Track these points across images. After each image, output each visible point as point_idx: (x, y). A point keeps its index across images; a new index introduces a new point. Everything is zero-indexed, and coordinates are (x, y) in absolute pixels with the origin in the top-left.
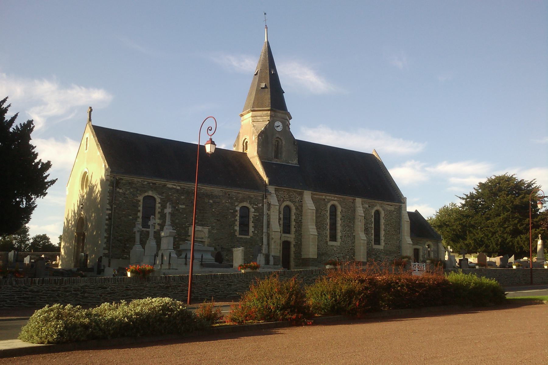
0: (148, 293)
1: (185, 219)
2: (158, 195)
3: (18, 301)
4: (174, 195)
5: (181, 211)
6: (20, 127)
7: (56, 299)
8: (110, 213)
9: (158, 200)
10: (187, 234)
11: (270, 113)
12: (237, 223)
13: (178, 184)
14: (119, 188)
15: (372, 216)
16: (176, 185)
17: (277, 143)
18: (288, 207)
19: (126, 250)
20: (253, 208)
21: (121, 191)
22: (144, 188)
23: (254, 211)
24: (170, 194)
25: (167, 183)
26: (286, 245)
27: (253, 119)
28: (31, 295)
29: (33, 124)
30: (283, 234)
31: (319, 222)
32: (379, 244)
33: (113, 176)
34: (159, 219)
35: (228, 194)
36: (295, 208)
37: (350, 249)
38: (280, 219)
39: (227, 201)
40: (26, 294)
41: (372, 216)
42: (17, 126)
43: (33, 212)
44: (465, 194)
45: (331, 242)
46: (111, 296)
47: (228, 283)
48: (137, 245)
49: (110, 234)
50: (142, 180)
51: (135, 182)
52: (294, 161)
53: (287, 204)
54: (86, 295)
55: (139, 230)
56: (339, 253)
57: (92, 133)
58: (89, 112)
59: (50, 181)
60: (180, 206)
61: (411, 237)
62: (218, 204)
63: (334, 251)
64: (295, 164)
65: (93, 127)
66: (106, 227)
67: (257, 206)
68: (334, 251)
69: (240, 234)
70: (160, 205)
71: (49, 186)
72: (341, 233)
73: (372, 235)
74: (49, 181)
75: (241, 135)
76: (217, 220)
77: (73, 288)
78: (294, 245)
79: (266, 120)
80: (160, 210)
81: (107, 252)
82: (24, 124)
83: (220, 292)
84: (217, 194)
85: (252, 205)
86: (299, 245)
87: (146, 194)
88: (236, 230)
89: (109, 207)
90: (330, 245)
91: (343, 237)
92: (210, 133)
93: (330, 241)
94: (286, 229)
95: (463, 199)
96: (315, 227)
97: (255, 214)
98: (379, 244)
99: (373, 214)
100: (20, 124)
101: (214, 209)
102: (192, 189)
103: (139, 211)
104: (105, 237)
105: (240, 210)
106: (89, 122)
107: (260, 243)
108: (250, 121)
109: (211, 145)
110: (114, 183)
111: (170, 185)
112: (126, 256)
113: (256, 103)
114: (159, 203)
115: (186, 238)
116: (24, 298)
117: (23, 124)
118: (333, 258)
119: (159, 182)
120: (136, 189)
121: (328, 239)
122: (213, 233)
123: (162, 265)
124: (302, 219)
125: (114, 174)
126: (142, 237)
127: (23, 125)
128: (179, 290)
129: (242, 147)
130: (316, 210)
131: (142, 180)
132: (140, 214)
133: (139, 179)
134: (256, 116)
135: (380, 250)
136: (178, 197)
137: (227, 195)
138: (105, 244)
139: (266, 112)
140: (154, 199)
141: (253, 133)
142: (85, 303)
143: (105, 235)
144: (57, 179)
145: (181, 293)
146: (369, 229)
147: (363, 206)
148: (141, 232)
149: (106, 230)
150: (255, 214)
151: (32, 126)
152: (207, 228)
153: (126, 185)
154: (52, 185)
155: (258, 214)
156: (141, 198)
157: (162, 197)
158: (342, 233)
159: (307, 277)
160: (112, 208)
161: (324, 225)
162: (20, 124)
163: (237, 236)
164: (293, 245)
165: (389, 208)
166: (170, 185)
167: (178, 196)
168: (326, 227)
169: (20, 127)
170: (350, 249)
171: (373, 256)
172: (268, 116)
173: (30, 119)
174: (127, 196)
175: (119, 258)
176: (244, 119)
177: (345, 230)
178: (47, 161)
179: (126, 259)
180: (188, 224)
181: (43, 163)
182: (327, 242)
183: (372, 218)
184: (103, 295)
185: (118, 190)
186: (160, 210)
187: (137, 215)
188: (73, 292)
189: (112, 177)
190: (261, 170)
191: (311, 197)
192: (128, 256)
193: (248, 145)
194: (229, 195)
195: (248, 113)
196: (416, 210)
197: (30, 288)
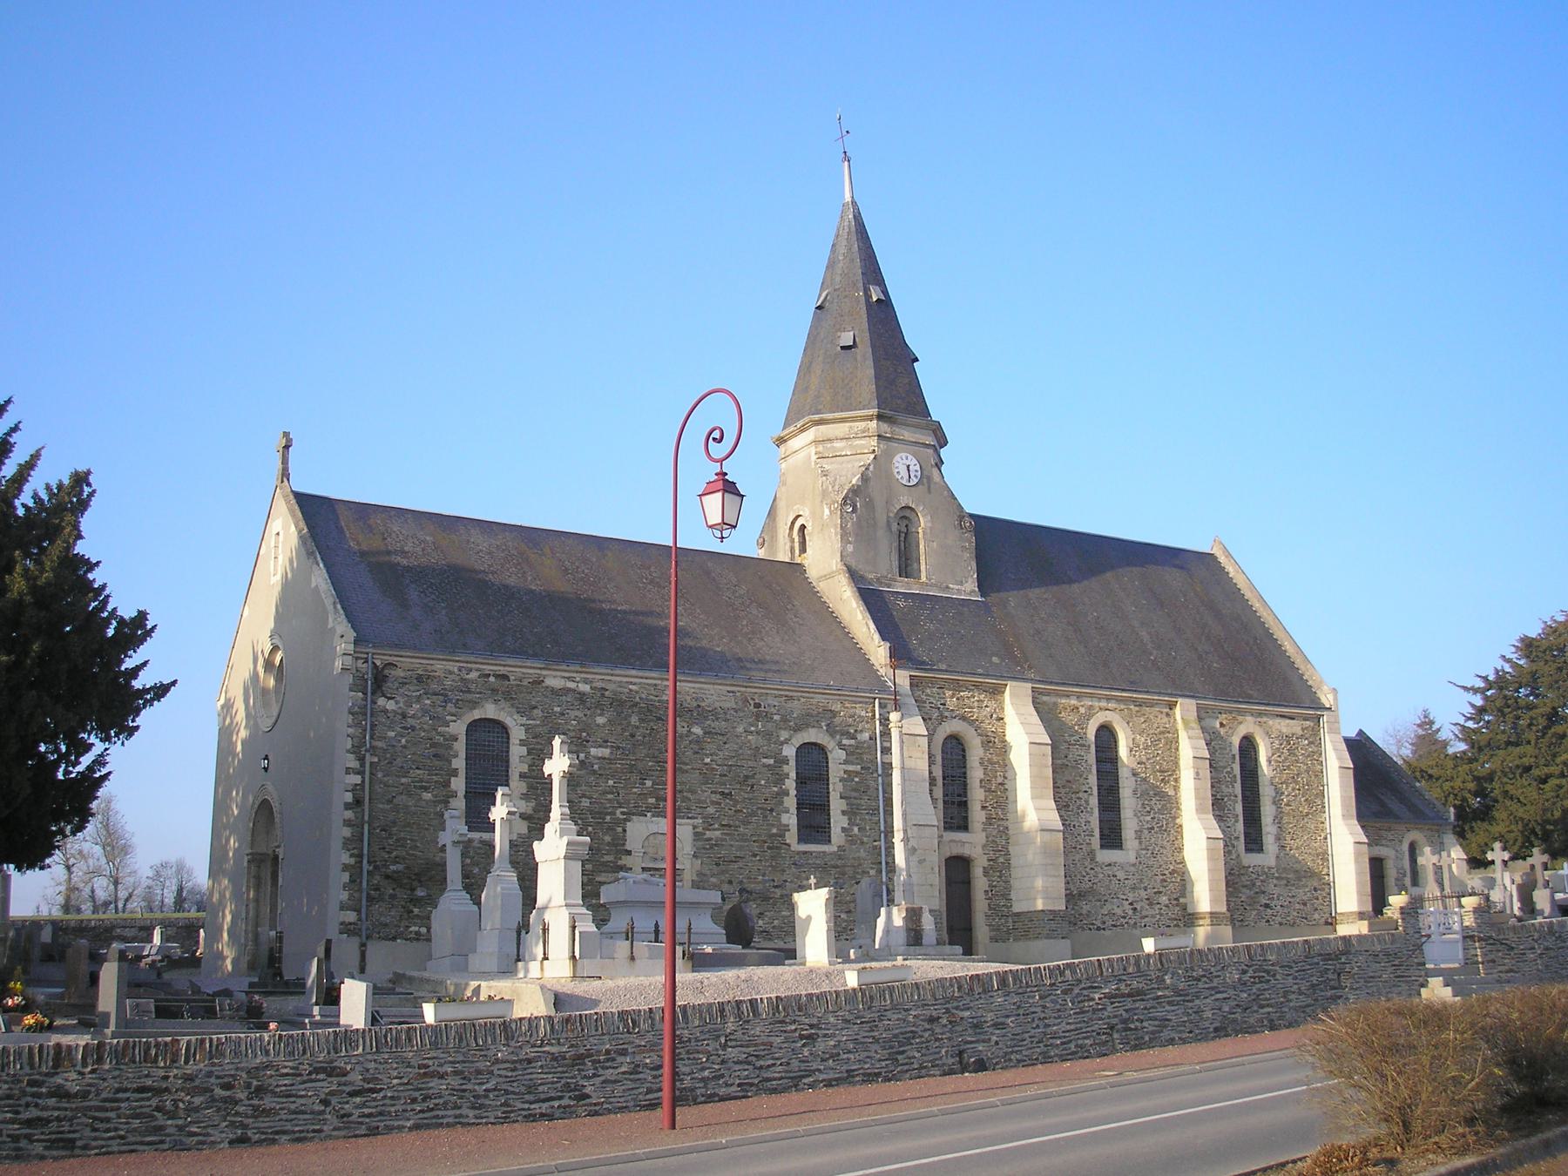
0: (504, 1087)
1: (610, 796)
2: (515, 717)
3: (8, 1136)
4: (573, 714)
5: (596, 767)
6: (45, 497)
7: (153, 1124)
8: (359, 782)
9: (517, 733)
10: (622, 850)
11: (875, 425)
12: (791, 802)
13: (583, 675)
14: (384, 696)
15: (1234, 755)
16: (578, 679)
17: (907, 526)
18: (957, 739)
19: (416, 911)
20: (841, 746)
21: (391, 705)
22: (469, 692)
23: (844, 758)
24: (557, 709)
25: (544, 672)
26: (957, 870)
27: (820, 448)
28: (58, 1109)
29: (89, 485)
30: (944, 834)
31: (1064, 787)
32: (1260, 850)
33: (366, 656)
34: (521, 798)
35: (752, 702)
36: (980, 742)
37: (1170, 873)
38: (932, 781)
39: (752, 729)
40: (36, 1105)
41: (1234, 755)
42: (36, 496)
43: (99, 794)
44: (1480, 677)
45: (1105, 852)
46: (364, 1105)
47: (803, 1030)
48: (450, 894)
49: (360, 856)
50: (462, 665)
51: (437, 674)
52: (967, 582)
53: (953, 729)
54: (268, 1102)
55: (456, 838)
56: (1134, 888)
57: (294, 516)
58: (281, 450)
59: (151, 688)
60: (593, 751)
61: (1359, 821)
62: (721, 738)
63: (1119, 880)
64: (970, 594)
65: (295, 497)
66: (347, 832)
67: (853, 742)
68: (1119, 880)
69: (801, 840)
70: (524, 750)
71: (150, 702)
72: (1136, 820)
73: (1237, 821)
74: (148, 687)
75: (781, 504)
76: (722, 793)
77: (218, 1077)
78: (984, 868)
79: (866, 451)
80: (525, 768)
81: (351, 916)
82: (60, 486)
83: (774, 1065)
84: (717, 705)
85: (838, 737)
86: (1000, 867)
87: (477, 714)
88: (786, 828)
89: (355, 764)
90: (1103, 863)
91: (1146, 832)
92: (718, 450)
93: (1102, 847)
94: (956, 814)
95: (1475, 690)
96: (1053, 805)
97: (851, 768)
98: (1260, 850)
99: (1236, 750)
100: (48, 487)
101: (707, 756)
102: (631, 690)
103: (455, 773)
104: (346, 868)
105: (797, 756)
106: (282, 482)
107: (872, 868)
108: (810, 457)
109: (726, 495)
110: (366, 680)
111: (554, 681)
112: (417, 929)
113: (828, 398)
114: (522, 743)
115: (620, 863)
116: (29, 1123)
117: (55, 486)
118: (1115, 907)
119: (521, 670)
120: (441, 698)
121: (1096, 840)
122: (711, 839)
123: (545, 962)
124: (1005, 778)
125: (367, 650)
126: (468, 861)
127: (56, 491)
128: (623, 1069)
129: (785, 544)
130: (1051, 745)
131: (462, 665)
132: (459, 784)
133: (451, 663)
134: (829, 440)
135: (1266, 870)
136: (584, 719)
137: (752, 707)
138: (344, 890)
139: (862, 425)
140: (504, 729)
141: (824, 493)
142: (266, 1133)
143: (346, 858)
144: (174, 683)
145: (631, 1080)
146: (1226, 799)
147: (1203, 723)
148: (466, 847)
149: (347, 843)
150: (851, 768)
151: (87, 490)
152: (688, 824)
153: (406, 684)
154: (159, 701)
155: (859, 767)
156: (459, 728)
157: (531, 722)
158: (1142, 818)
159: (1084, 989)
160: (363, 765)
161: (1081, 795)
162: (48, 487)
163: (792, 849)
164: (981, 869)
165: (1284, 726)
166: (554, 681)
167: (585, 715)
168: (1087, 802)
169: (45, 497)
170: (1170, 873)
171: (1244, 890)
172: (870, 437)
173: (82, 468)
174: (411, 722)
175: (394, 939)
176: (787, 454)
177: (1148, 809)
178: (124, 604)
179: (418, 940)
180: (623, 813)
181: (122, 621)
182: (1092, 854)
183: (1233, 763)
184: (334, 1100)
185: (381, 701)
186: (527, 766)
187: (450, 786)
188: (219, 1092)
189: (362, 659)
190: (860, 617)
191: (1033, 702)
192: (424, 930)
193: (807, 538)
194: (758, 706)
195: (802, 431)
196: (1361, 730)
197: (52, 1080)
